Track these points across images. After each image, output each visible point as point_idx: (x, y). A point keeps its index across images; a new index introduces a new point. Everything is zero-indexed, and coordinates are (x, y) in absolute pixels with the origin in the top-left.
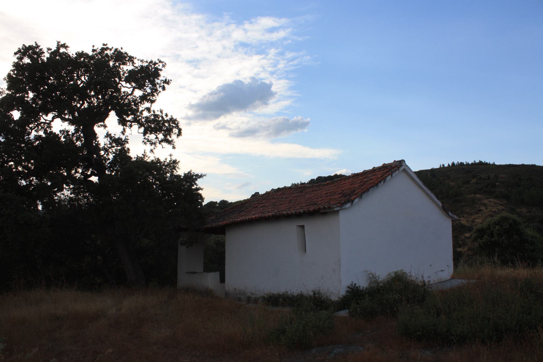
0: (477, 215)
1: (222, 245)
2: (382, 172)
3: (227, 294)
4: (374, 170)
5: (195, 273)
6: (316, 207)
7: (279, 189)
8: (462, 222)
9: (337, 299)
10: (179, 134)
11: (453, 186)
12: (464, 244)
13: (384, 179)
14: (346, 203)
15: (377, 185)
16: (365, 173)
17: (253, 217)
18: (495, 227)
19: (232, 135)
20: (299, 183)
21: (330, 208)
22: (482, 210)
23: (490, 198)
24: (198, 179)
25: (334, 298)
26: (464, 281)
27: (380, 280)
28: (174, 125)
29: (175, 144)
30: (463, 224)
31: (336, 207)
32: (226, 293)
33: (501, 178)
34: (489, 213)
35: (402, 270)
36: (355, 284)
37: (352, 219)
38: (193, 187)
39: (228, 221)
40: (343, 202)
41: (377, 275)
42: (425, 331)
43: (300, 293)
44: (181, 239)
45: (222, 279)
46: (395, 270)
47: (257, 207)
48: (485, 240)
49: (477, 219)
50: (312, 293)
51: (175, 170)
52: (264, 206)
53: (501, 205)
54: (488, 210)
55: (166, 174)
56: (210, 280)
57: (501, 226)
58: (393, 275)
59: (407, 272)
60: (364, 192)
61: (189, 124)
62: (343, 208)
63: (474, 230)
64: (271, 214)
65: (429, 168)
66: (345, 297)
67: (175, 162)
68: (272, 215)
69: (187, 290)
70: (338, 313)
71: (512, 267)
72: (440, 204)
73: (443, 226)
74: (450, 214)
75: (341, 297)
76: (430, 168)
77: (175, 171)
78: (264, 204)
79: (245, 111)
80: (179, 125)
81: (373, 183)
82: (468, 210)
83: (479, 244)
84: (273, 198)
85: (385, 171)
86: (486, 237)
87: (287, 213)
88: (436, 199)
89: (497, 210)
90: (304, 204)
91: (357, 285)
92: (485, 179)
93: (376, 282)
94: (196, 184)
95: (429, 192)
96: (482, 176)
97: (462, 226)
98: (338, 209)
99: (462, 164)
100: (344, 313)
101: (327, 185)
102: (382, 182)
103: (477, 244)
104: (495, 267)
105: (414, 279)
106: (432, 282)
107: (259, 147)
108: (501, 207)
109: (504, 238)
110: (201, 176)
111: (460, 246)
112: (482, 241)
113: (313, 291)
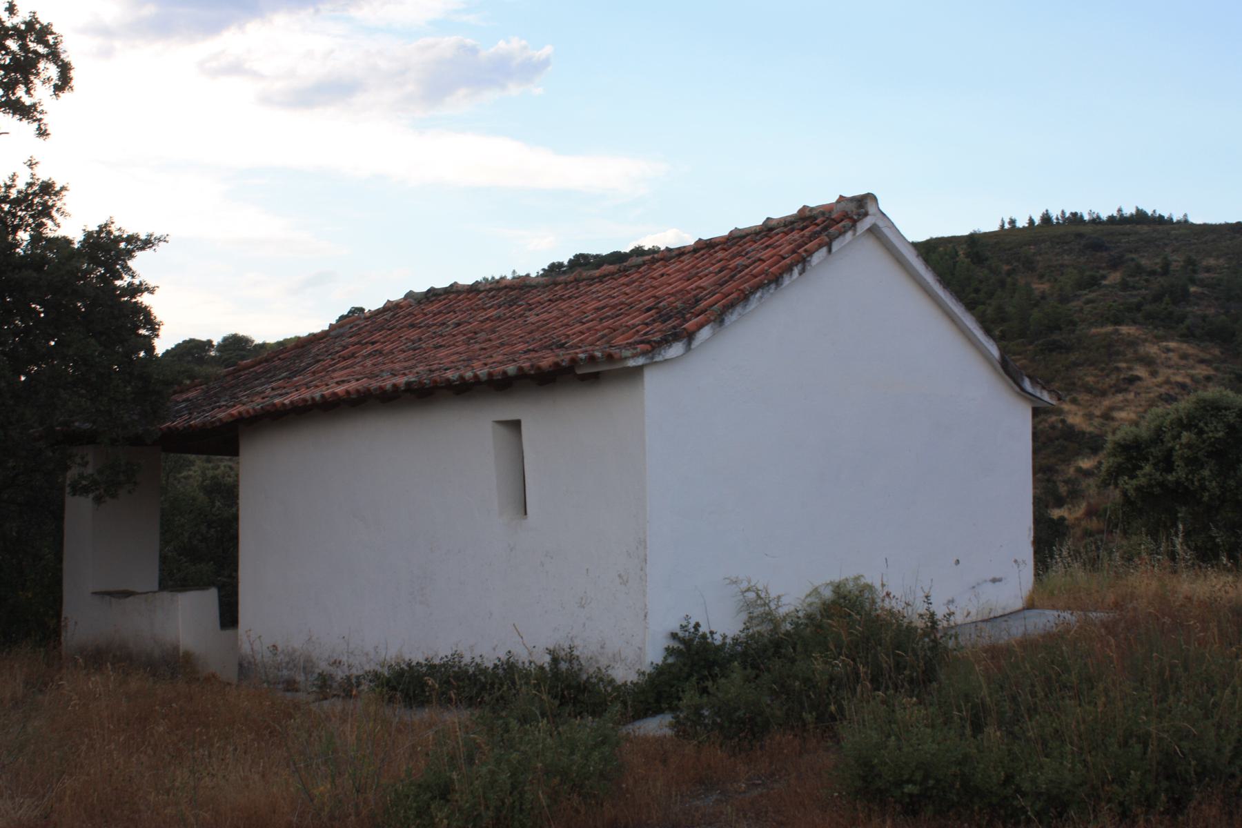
0: (1120, 397)
1: (229, 493)
2: (795, 235)
3: (245, 668)
4: (768, 229)
5: (127, 594)
6: (563, 357)
7: (432, 294)
8: (1071, 420)
9: (632, 677)
10: (64, 83)
11: (1039, 293)
12: (1075, 495)
13: (803, 261)
14: (666, 341)
15: (776, 280)
16: (737, 239)
17: (340, 389)
18: (1179, 436)
19: (266, 100)
20: (509, 277)
21: (610, 358)
22: (1138, 378)
23: (1165, 338)
24: (138, 254)
25: (624, 674)
26: (1067, 615)
27: (782, 611)
28: (41, 49)
29: (46, 119)
30: (1072, 427)
31: (634, 356)
32: (241, 665)
33: (1208, 269)
34: (1163, 390)
35: (857, 579)
36: (697, 626)
37: (687, 397)
38: (118, 283)
39: (249, 407)
40: (657, 338)
41: (773, 595)
42: (931, 782)
43: (504, 658)
44: (73, 473)
45: (229, 616)
46: (836, 578)
47: (353, 355)
48: (1143, 481)
49: (1121, 409)
50: (548, 658)
51: (51, 218)
52: (380, 352)
53: (1202, 361)
54: (1160, 379)
55: (16, 229)
56: (186, 619)
57: (1201, 432)
58: (828, 594)
59: (878, 586)
60: (732, 306)
61: (107, 53)
62: (657, 359)
63: (1109, 446)
64: (405, 379)
65: (963, 231)
66: (660, 671)
67: (47, 188)
68: (408, 384)
69: (96, 657)
70: (637, 724)
71: (1229, 571)
72: (995, 351)
73: (1001, 429)
74: (1027, 384)
75: (648, 670)
76: (966, 233)
77: (49, 223)
78: (378, 346)
79: (317, 11)
80: (61, 47)
81: (762, 272)
82: (1090, 379)
83: (1125, 493)
84: (412, 326)
85: (807, 232)
86: (1148, 468)
87: (461, 378)
88: (979, 334)
89: (1188, 381)
90: (521, 346)
91: (703, 629)
92: (1153, 273)
93: (769, 617)
94: (128, 270)
95: (958, 309)
96: (1143, 262)
97: (1070, 434)
98: (640, 361)
99: (1076, 219)
100: (656, 726)
101: (601, 279)
102: (796, 271)
103: (1115, 494)
104: (1175, 572)
105: (898, 606)
106: (959, 618)
107: (377, 145)
108: (1201, 371)
109: (1206, 473)
110: (147, 243)
111: (1060, 503)
112: (1134, 482)
113: (550, 652)
